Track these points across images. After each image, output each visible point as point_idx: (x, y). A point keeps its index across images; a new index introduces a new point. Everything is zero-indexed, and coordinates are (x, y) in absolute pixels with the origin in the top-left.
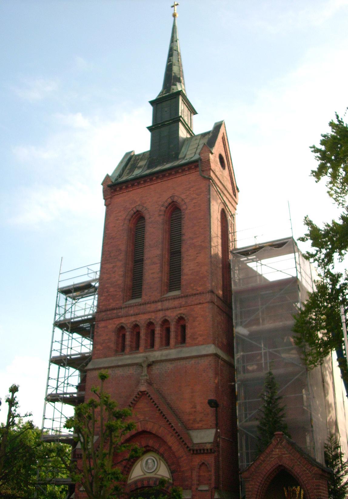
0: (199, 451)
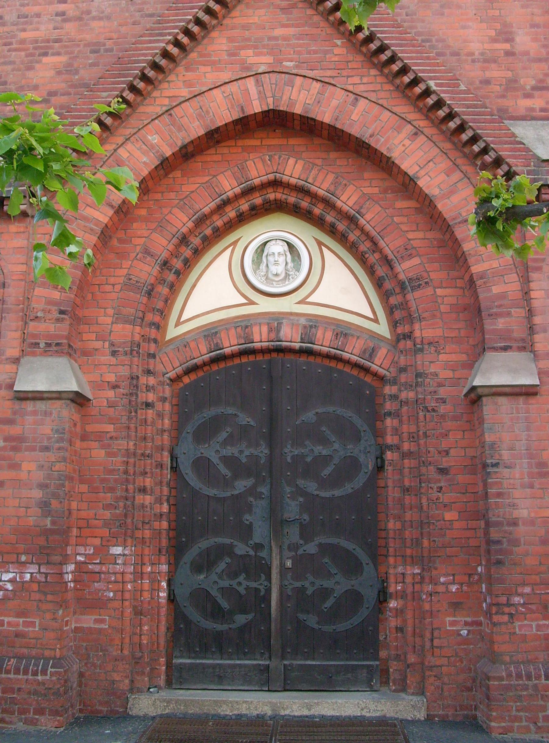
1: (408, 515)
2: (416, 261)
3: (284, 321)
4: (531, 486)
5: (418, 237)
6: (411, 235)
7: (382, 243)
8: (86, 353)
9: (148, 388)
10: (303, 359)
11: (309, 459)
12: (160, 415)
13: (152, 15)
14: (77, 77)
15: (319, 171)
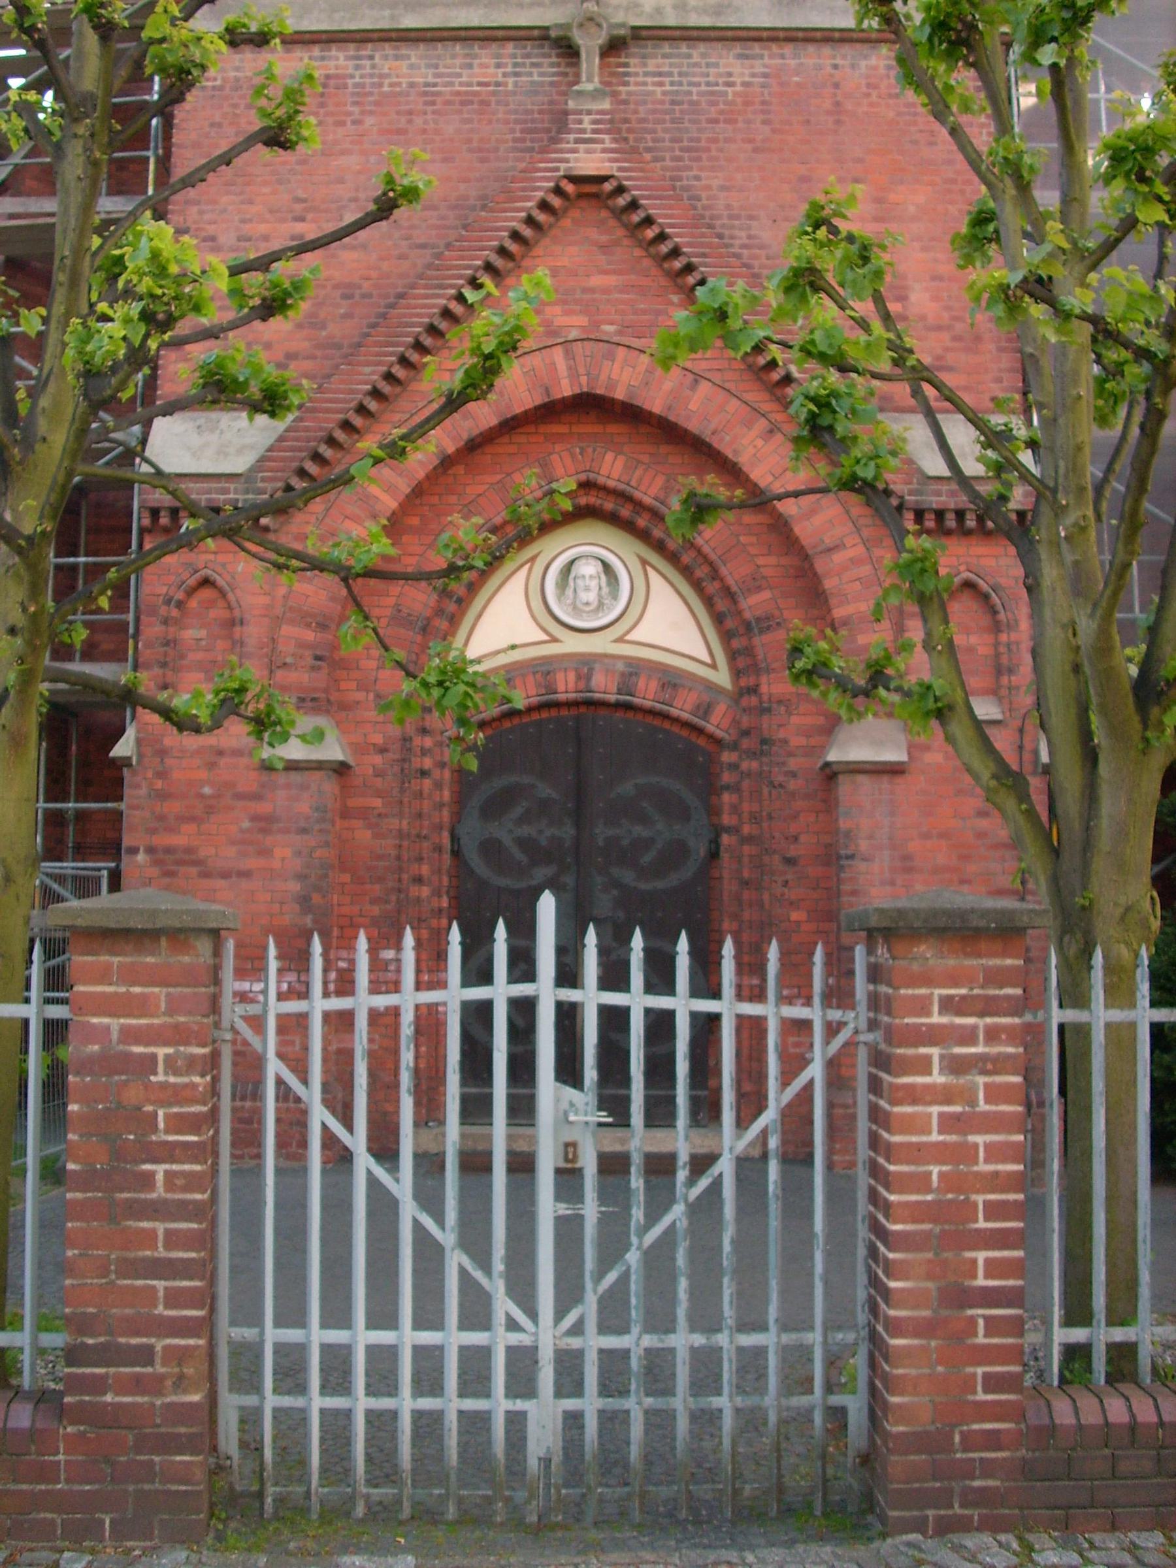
0: (951, 522)
1: (746, 915)
2: (766, 595)
3: (597, 666)
4: (892, 883)
5: (770, 564)
6: (761, 561)
7: (724, 571)
8: (344, 707)
9: (424, 752)
10: (619, 715)
11: (625, 842)
12: (438, 785)
13: (423, 246)
14: (324, 333)
15: (646, 470)
